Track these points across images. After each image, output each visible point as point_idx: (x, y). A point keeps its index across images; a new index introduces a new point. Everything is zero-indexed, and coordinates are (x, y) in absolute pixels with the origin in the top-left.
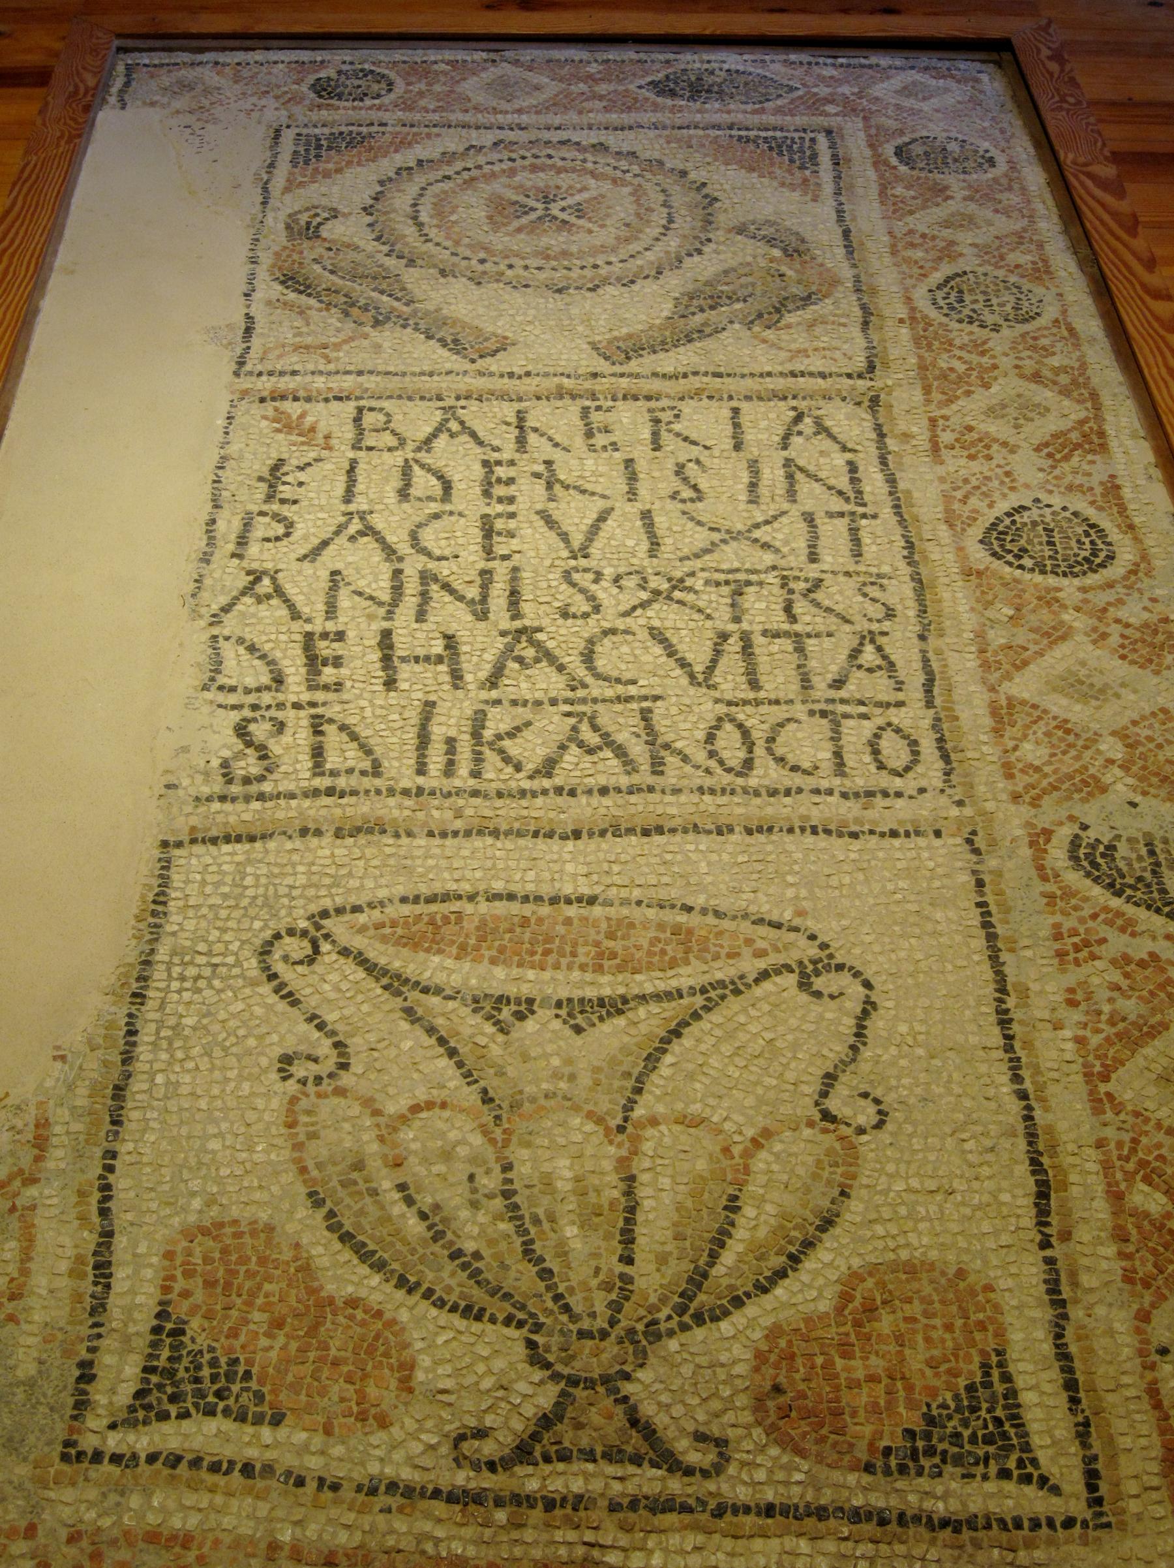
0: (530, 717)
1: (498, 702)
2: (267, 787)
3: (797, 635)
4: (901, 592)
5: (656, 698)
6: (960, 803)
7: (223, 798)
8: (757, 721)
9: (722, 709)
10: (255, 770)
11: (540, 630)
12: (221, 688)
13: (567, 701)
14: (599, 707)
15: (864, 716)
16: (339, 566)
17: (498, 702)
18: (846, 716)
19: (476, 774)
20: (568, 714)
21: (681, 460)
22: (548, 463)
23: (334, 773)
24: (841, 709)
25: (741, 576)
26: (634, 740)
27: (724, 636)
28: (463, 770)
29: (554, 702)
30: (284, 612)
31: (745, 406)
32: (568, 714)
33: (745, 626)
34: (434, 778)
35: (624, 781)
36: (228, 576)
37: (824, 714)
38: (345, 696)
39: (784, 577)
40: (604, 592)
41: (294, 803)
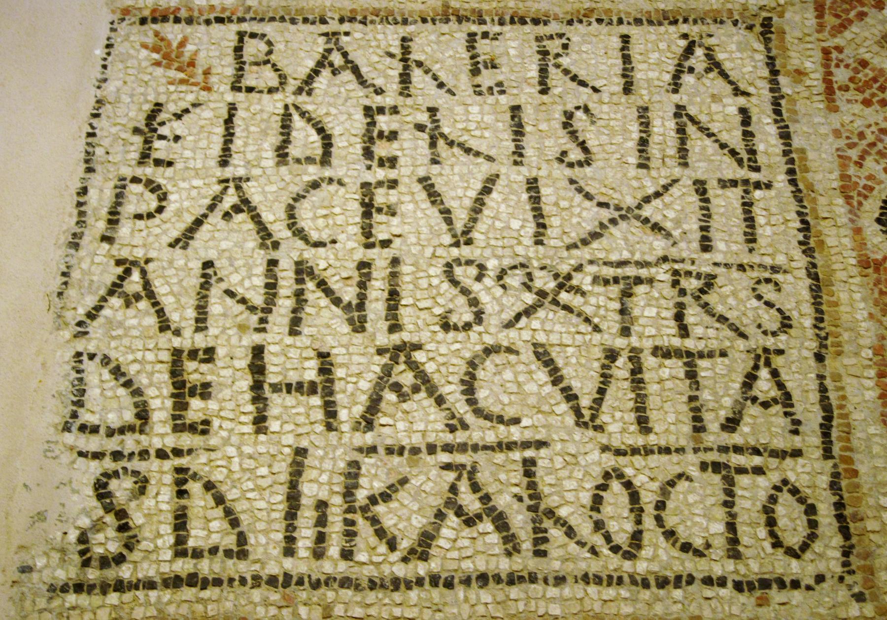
0: (405, 470)
1: (373, 450)
2: (125, 572)
3: (689, 354)
4: (795, 293)
5: (541, 444)
6: (859, 598)
7: (79, 588)
8: (646, 475)
9: (609, 461)
10: (114, 547)
11: (418, 347)
12: (83, 428)
13: (448, 448)
14: (481, 457)
15: (759, 471)
16: (212, 255)
17: (373, 450)
18: (741, 471)
19: (347, 555)
20: (447, 467)
21: (570, 107)
22: (433, 111)
23: (197, 554)
24: (736, 460)
25: (631, 271)
26: (516, 505)
27: (612, 355)
28: (334, 551)
29: (432, 449)
30: (152, 321)
31: (634, 31)
32: (447, 467)
33: (634, 341)
34: (300, 564)
35: (504, 565)
36: (97, 266)
37: (717, 467)
38: (213, 441)
39: (676, 273)
40: (487, 292)
41: (153, 594)
